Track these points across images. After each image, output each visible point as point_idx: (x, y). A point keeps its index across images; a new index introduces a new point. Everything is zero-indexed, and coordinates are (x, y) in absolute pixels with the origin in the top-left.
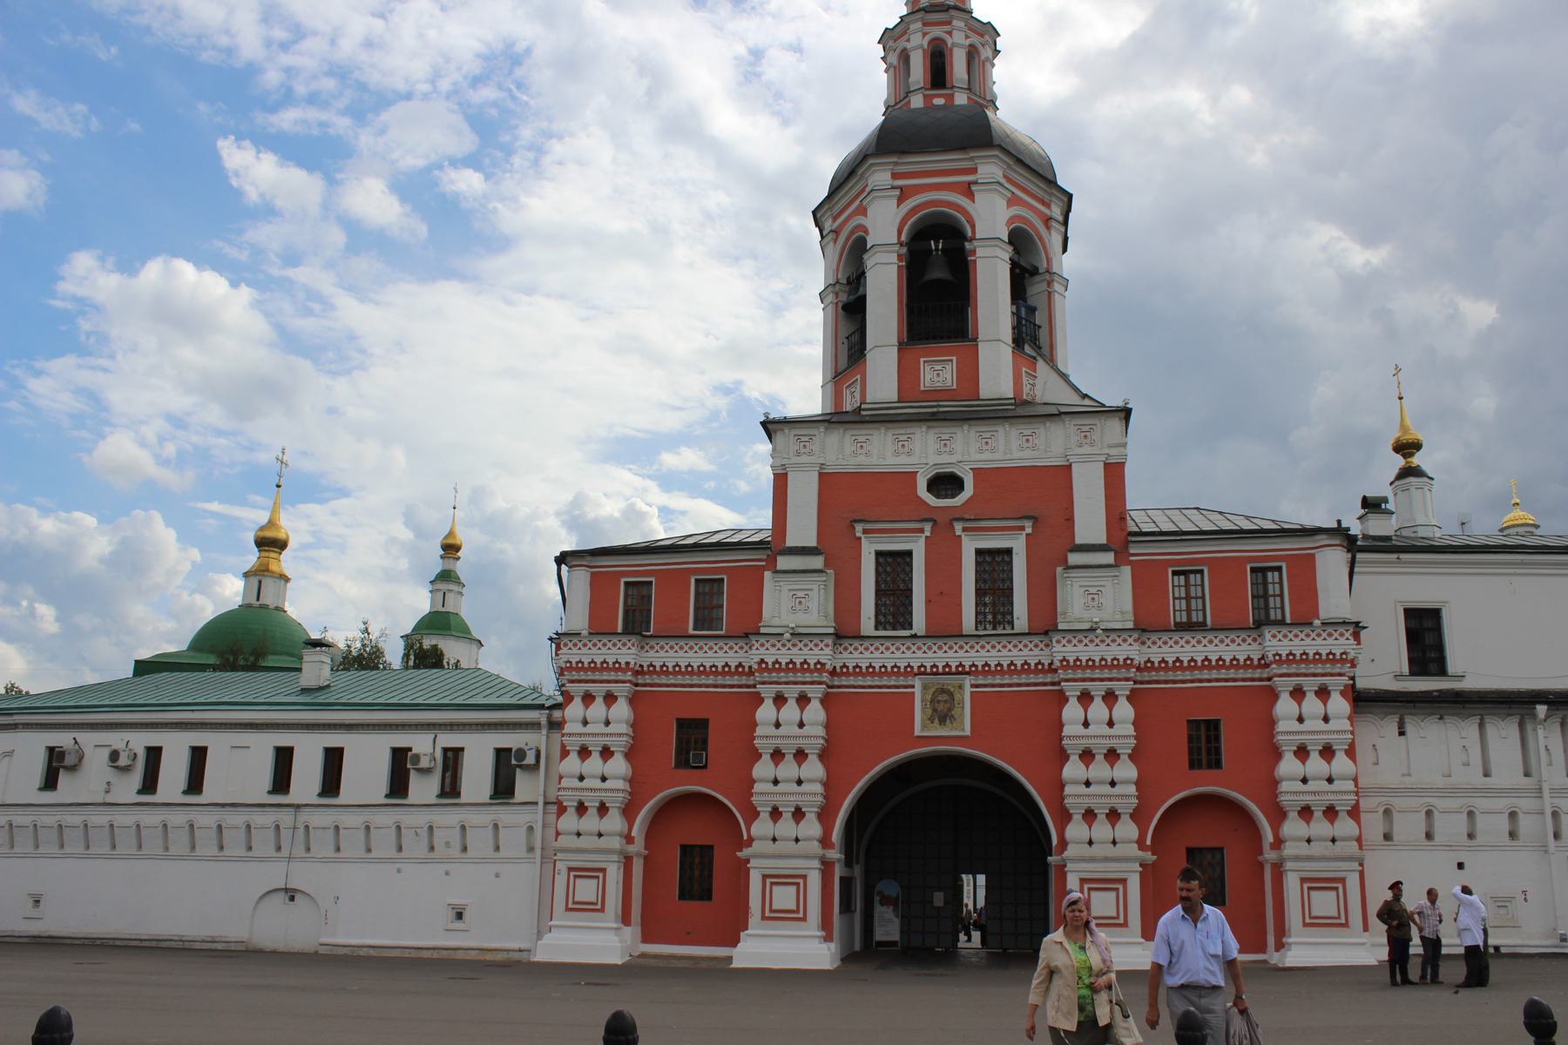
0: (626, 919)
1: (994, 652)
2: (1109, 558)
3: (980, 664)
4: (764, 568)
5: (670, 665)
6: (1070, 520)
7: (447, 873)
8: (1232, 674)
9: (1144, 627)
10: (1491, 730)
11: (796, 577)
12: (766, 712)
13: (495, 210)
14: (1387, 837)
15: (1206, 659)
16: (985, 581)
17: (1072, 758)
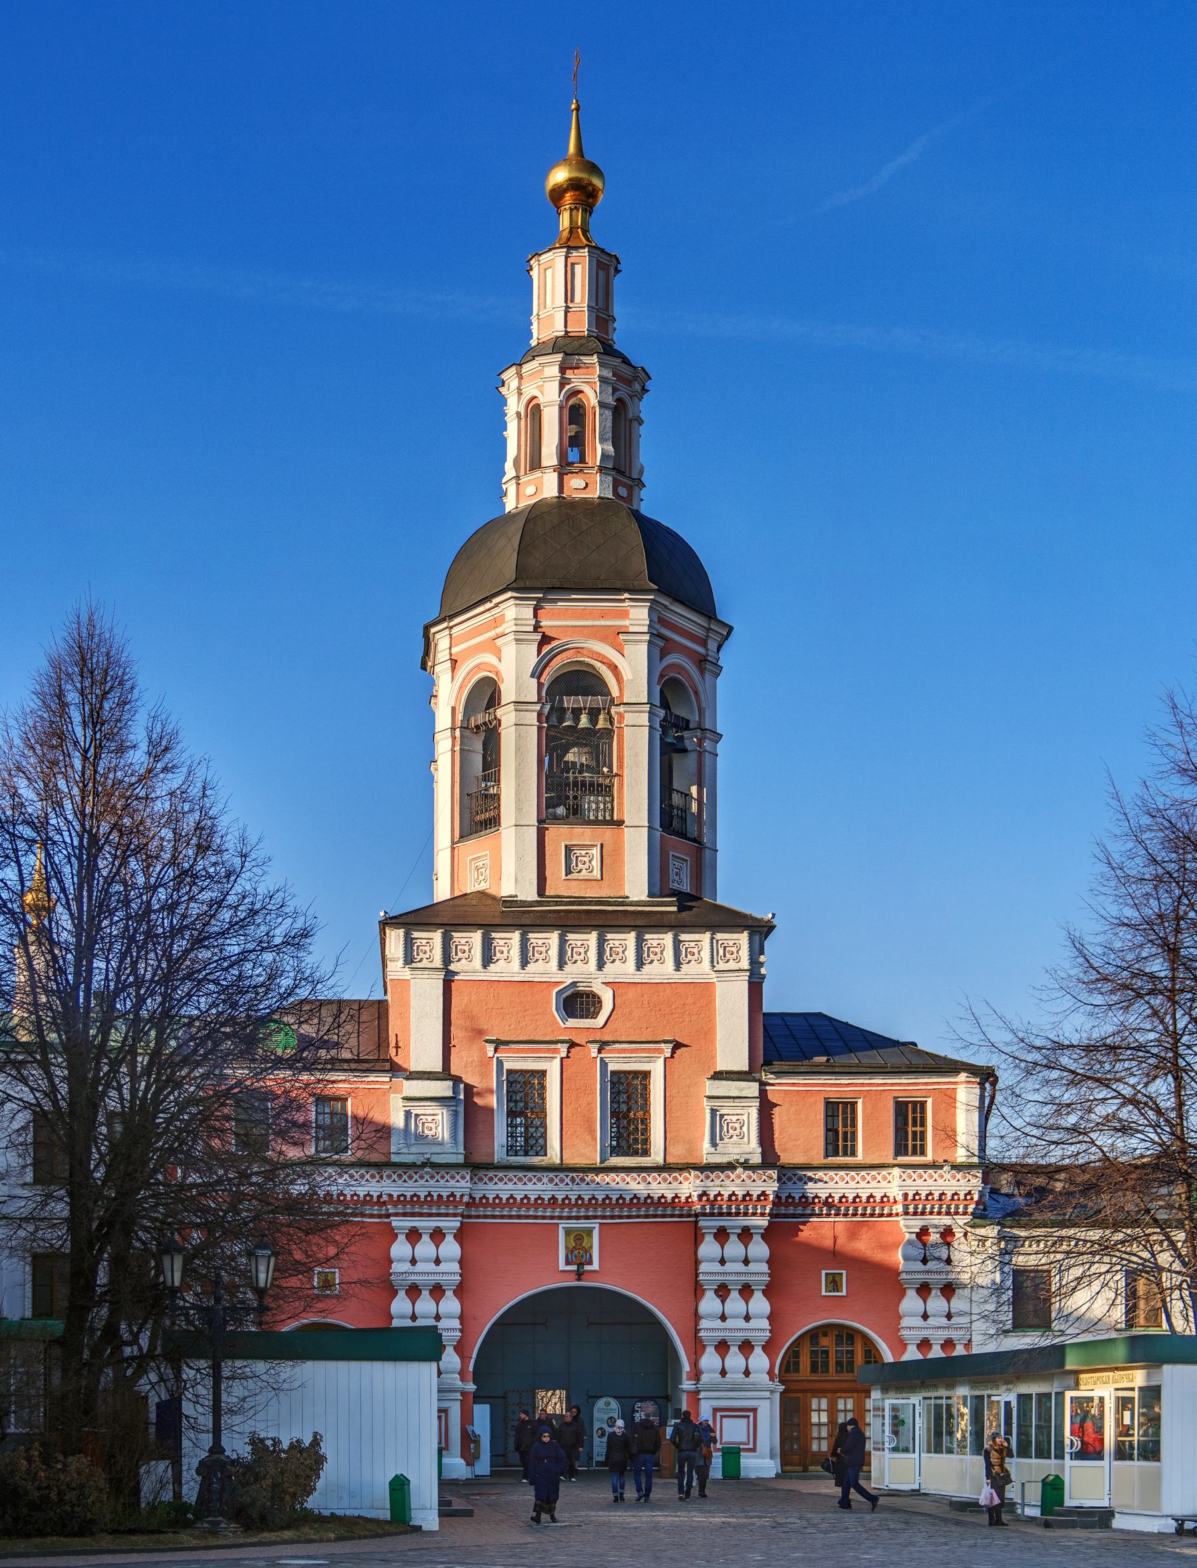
12: (400, 1249)
17: (933, 1292)
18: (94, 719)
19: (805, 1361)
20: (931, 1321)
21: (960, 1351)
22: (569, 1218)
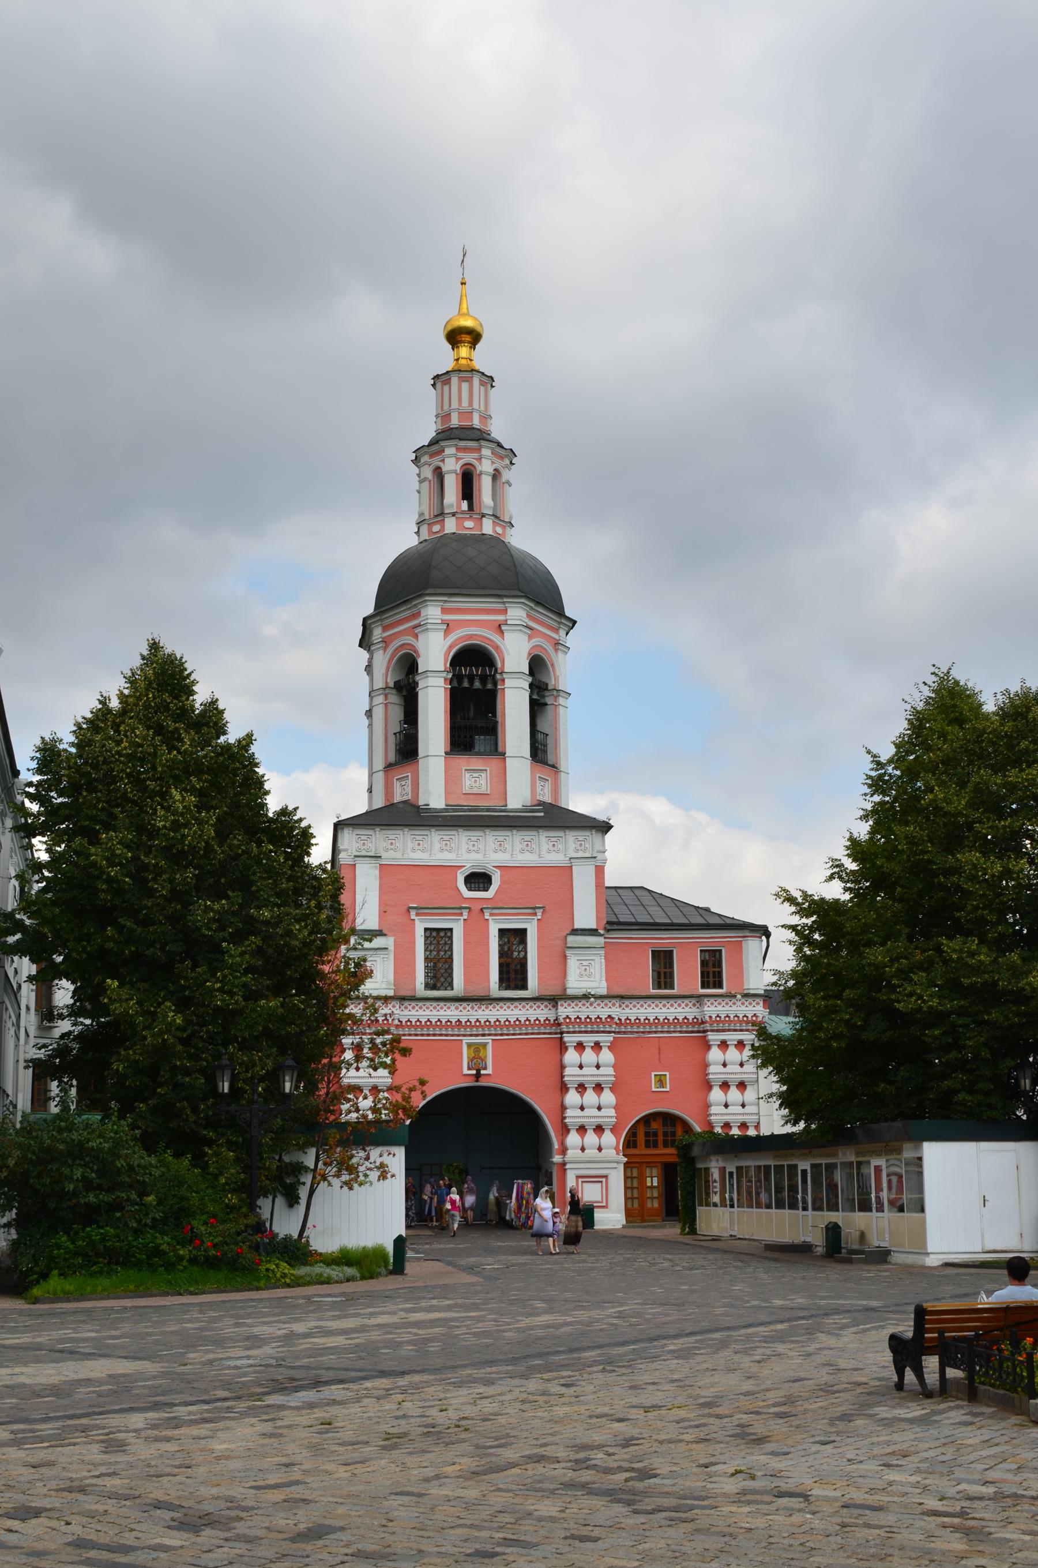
13: (48, 755)
18: (462, 1382)
19: (641, 1139)
21: (752, 1132)
22: (471, 1035)
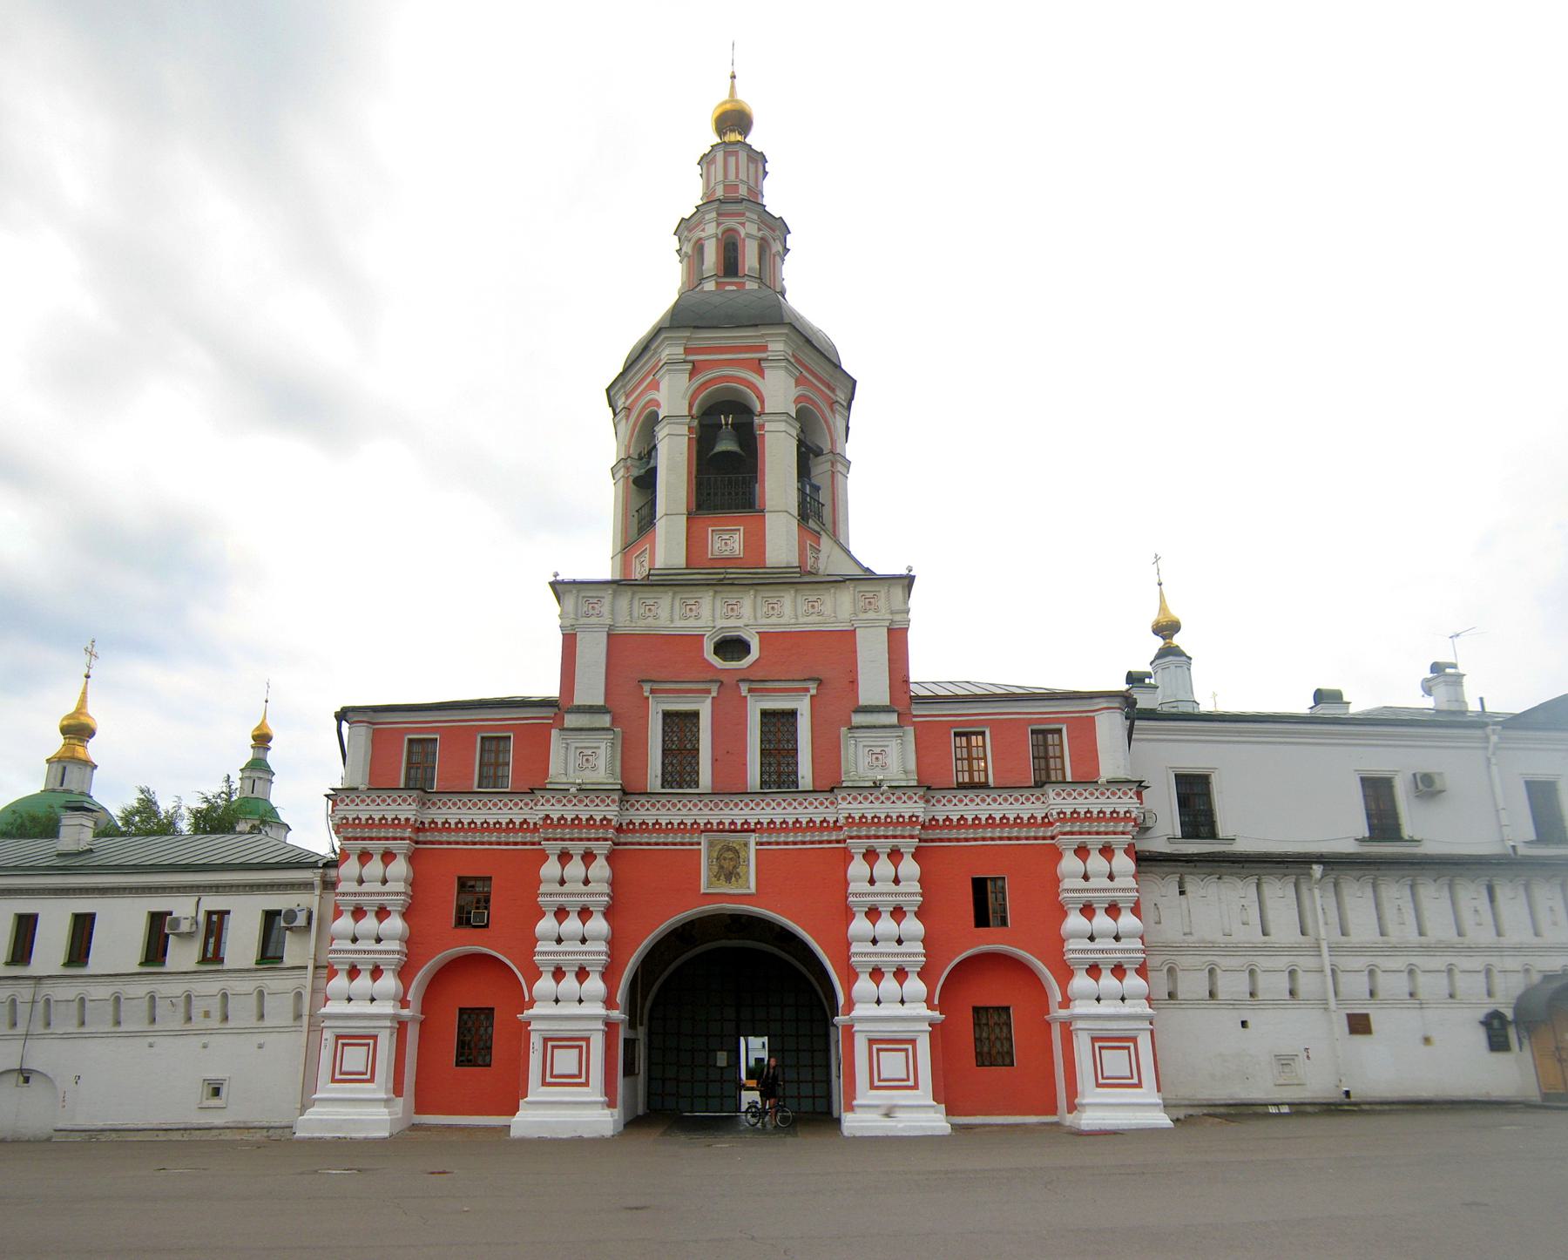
0: (398, 1090)
1: (779, 810)
2: (892, 719)
3: (765, 822)
4: (551, 726)
5: (453, 822)
6: (854, 682)
7: (205, 1047)
8: (1015, 832)
9: (927, 787)
10: (1267, 890)
11: (583, 735)
14: (1171, 995)
15: (990, 817)
16: (770, 742)
17: (1123, 912)
20: (567, 888)
